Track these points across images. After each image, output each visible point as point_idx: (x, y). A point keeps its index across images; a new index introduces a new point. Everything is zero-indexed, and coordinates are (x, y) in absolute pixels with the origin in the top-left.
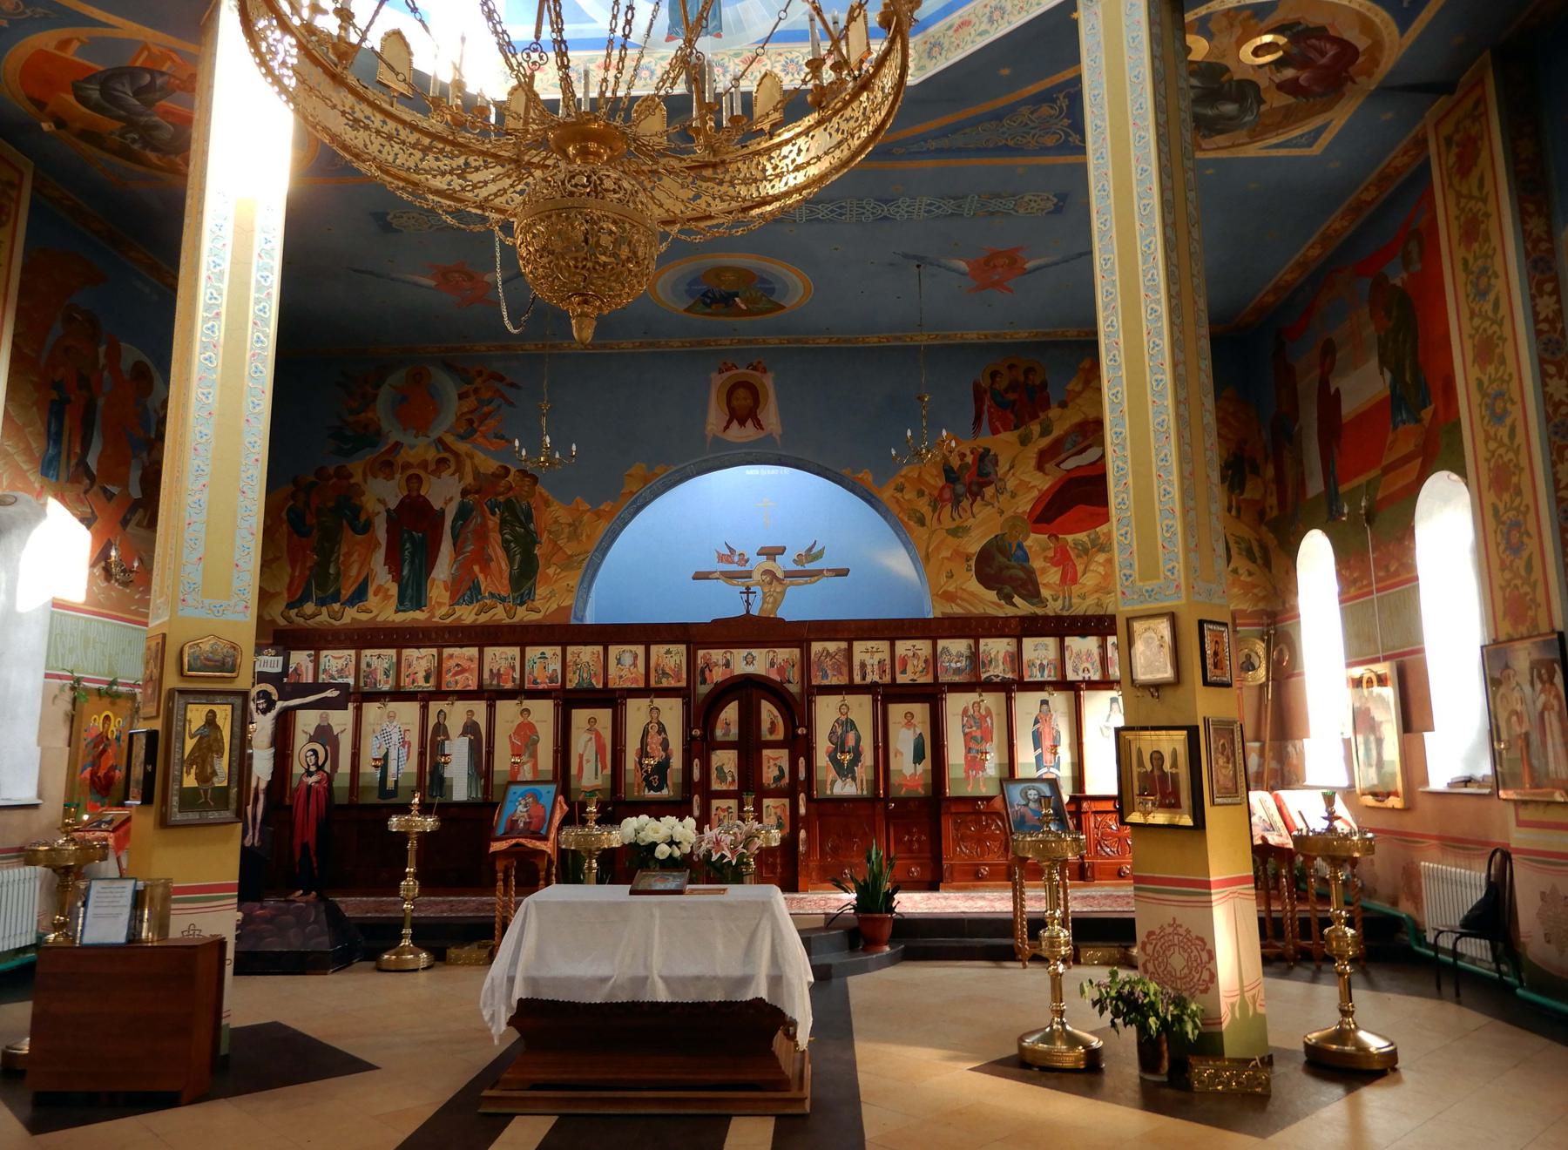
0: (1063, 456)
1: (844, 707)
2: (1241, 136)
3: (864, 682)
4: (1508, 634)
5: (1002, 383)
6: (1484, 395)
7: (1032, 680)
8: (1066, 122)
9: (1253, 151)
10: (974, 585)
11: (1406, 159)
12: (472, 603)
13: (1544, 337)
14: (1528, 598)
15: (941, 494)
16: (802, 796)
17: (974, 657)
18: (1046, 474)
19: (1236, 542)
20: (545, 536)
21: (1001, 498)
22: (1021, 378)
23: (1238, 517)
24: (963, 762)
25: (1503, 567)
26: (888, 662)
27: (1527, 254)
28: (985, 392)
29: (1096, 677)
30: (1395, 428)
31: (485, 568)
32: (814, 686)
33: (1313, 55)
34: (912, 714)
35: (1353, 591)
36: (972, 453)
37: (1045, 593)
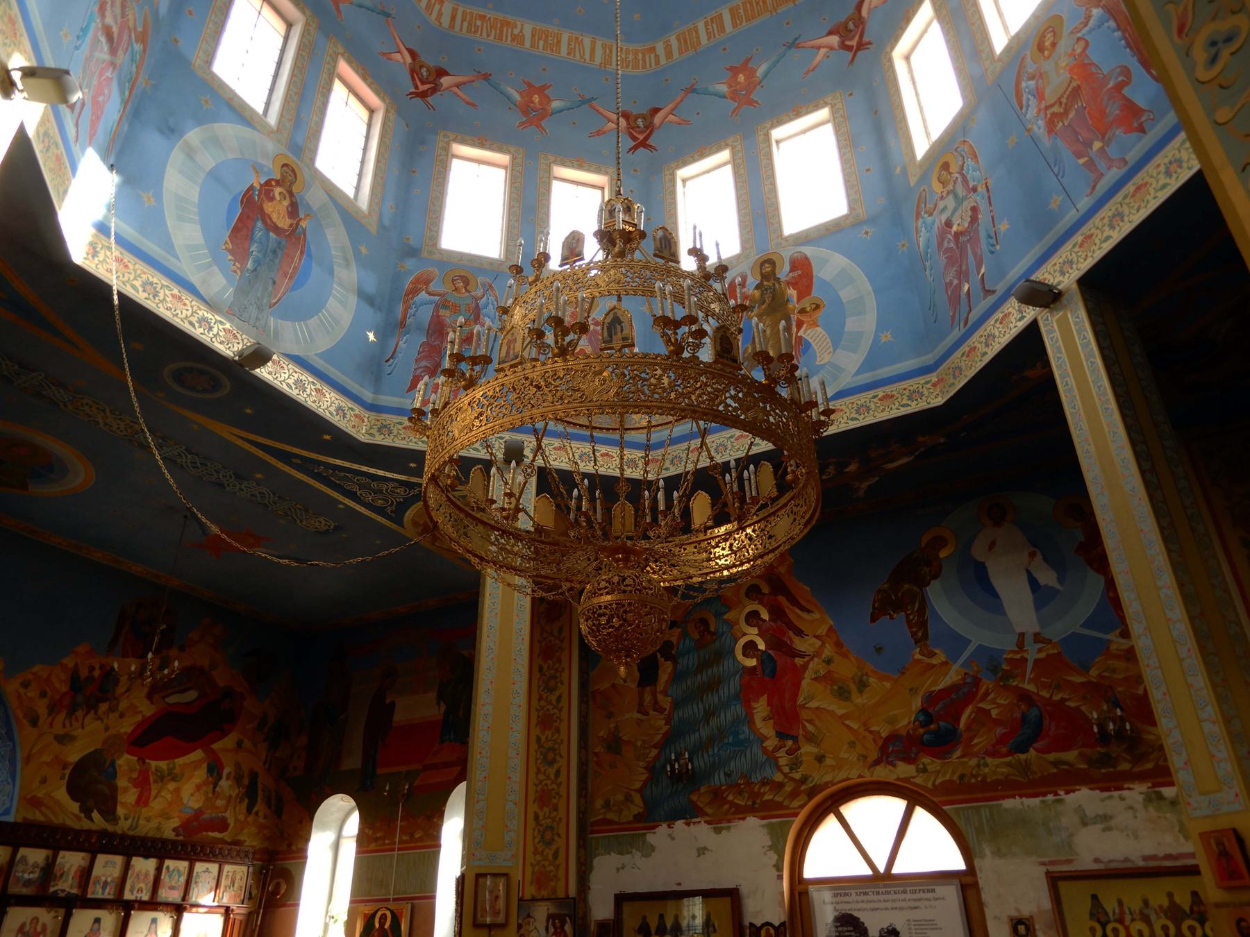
6: (541, 746)
7: (93, 896)
10: (62, 794)
14: (552, 874)
18: (152, 703)
19: (263, 791)
21: (111, 716)
25: (535, 852)
35: (373, 846)
36: (100, 668)
37: (120, 811)
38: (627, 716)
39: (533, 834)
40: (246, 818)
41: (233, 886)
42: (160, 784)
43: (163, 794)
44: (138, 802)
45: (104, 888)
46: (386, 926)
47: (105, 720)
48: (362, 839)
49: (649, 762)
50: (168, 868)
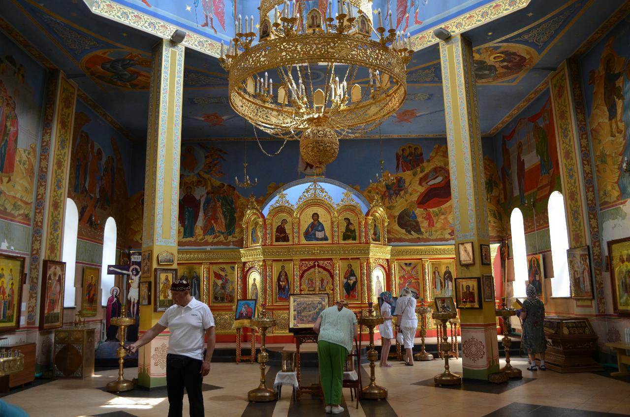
0: (428, 180)
2: (491, 80)
4: (574, 246)
5: (407, 152)
8: (433, 75)
9: (495, 83)
11: (543, 87)
12: (211, 234)
13: (583, 152)
15: (384, 194)
19: (490, 211)
20: (238, 210)
22: (413, 151)
23: (490, 202)
25: (573, 225)
27: (578, 126)
28: (400, 156)
30: (542, 175)
31: (216, 222)
33: (512, 59)
37: (423, 230)
38: (607, 140)
42: (437, 218)
43: (439, 221)
44: (429, 225)
47: (405, 197)
49: (619, 165)
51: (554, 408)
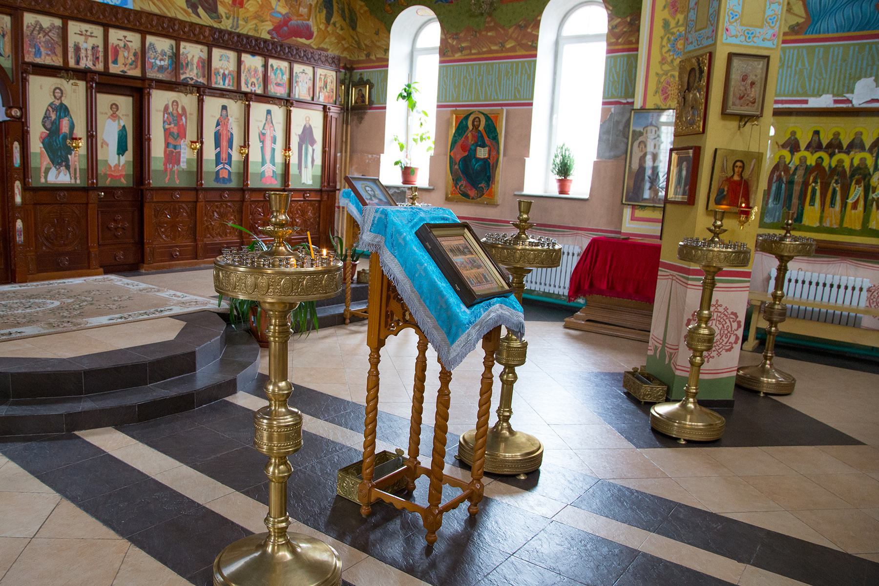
1: (58, 92)
3: (78, 67)
16: (18, 185)
17: (176, 56)
24: (163, 156)
26: (101, 49)
29: (259, 91)
32: (29, 64)
34: (117, 106)
37: (221, 10)
39: (661, 43)
40: (326, 27)
41: (326, 88)
45: (224, 80)
46: (481, 128)
48: (445, 51)
50: (272, 66)
51: (328, 442)
